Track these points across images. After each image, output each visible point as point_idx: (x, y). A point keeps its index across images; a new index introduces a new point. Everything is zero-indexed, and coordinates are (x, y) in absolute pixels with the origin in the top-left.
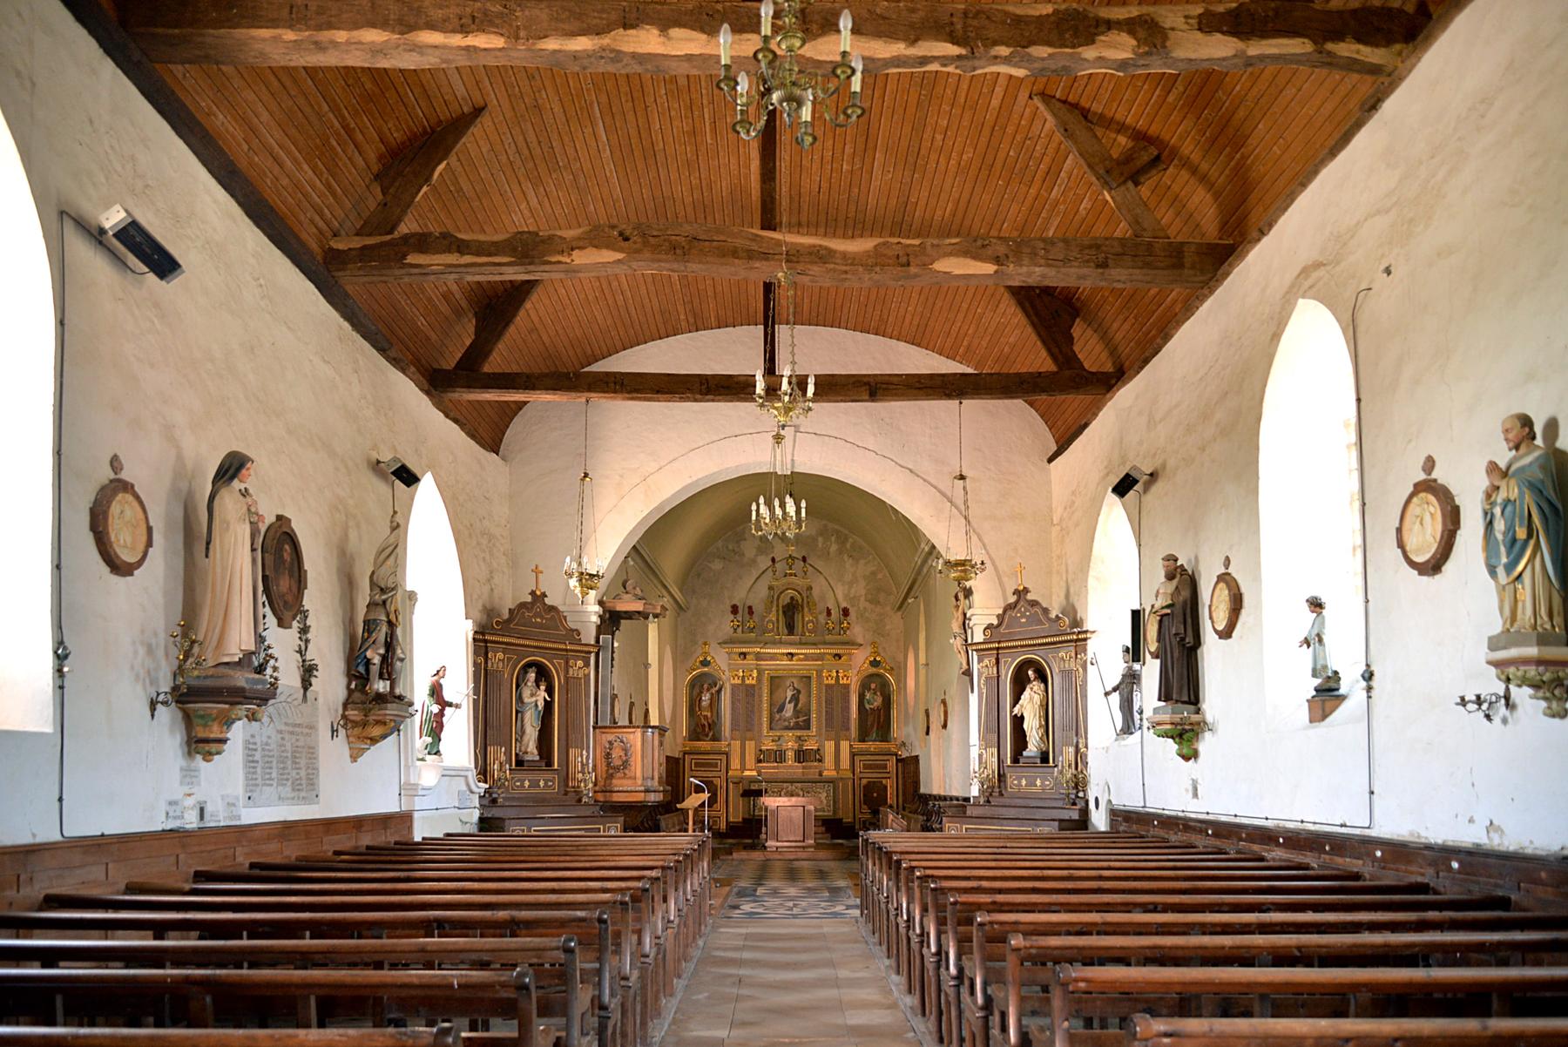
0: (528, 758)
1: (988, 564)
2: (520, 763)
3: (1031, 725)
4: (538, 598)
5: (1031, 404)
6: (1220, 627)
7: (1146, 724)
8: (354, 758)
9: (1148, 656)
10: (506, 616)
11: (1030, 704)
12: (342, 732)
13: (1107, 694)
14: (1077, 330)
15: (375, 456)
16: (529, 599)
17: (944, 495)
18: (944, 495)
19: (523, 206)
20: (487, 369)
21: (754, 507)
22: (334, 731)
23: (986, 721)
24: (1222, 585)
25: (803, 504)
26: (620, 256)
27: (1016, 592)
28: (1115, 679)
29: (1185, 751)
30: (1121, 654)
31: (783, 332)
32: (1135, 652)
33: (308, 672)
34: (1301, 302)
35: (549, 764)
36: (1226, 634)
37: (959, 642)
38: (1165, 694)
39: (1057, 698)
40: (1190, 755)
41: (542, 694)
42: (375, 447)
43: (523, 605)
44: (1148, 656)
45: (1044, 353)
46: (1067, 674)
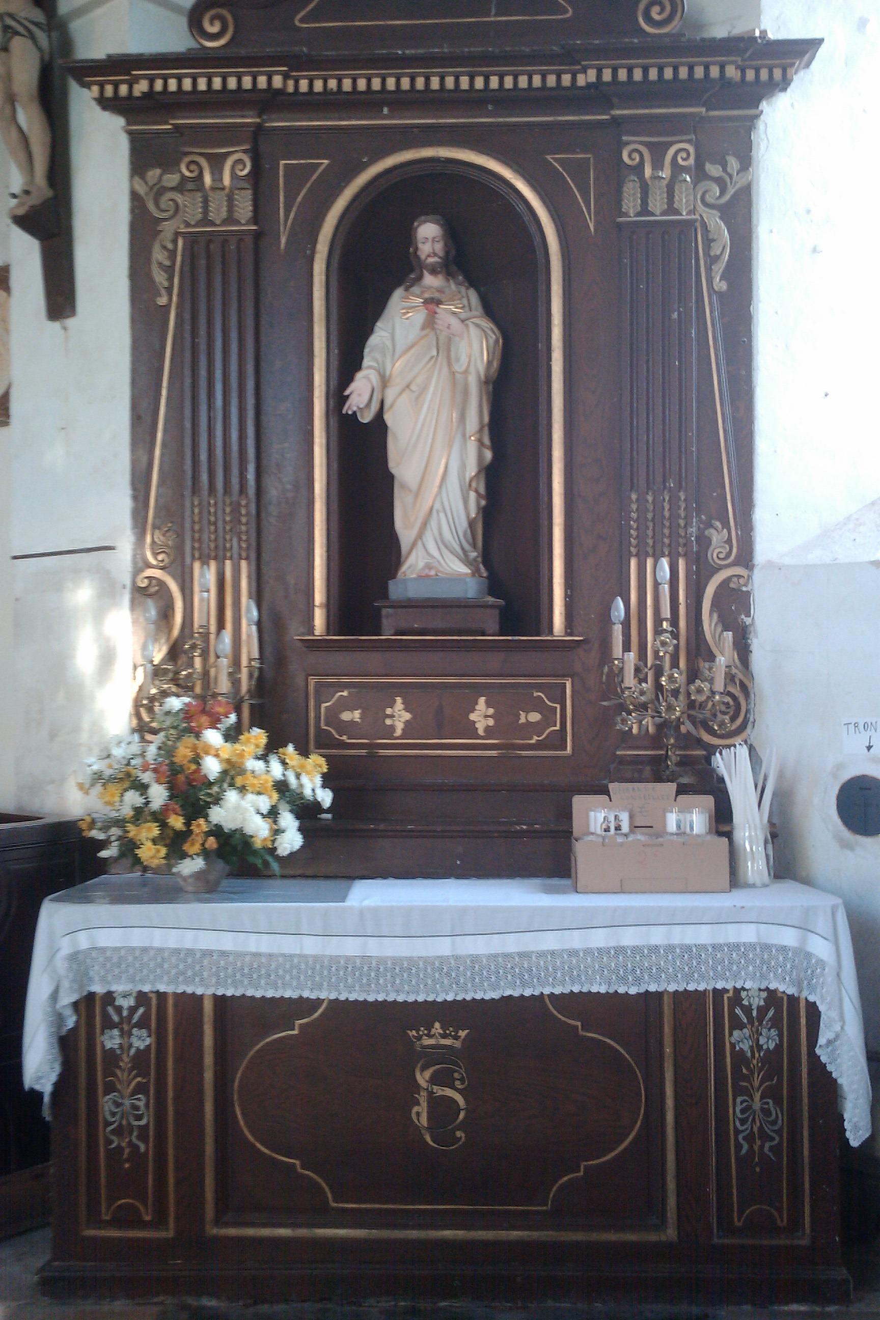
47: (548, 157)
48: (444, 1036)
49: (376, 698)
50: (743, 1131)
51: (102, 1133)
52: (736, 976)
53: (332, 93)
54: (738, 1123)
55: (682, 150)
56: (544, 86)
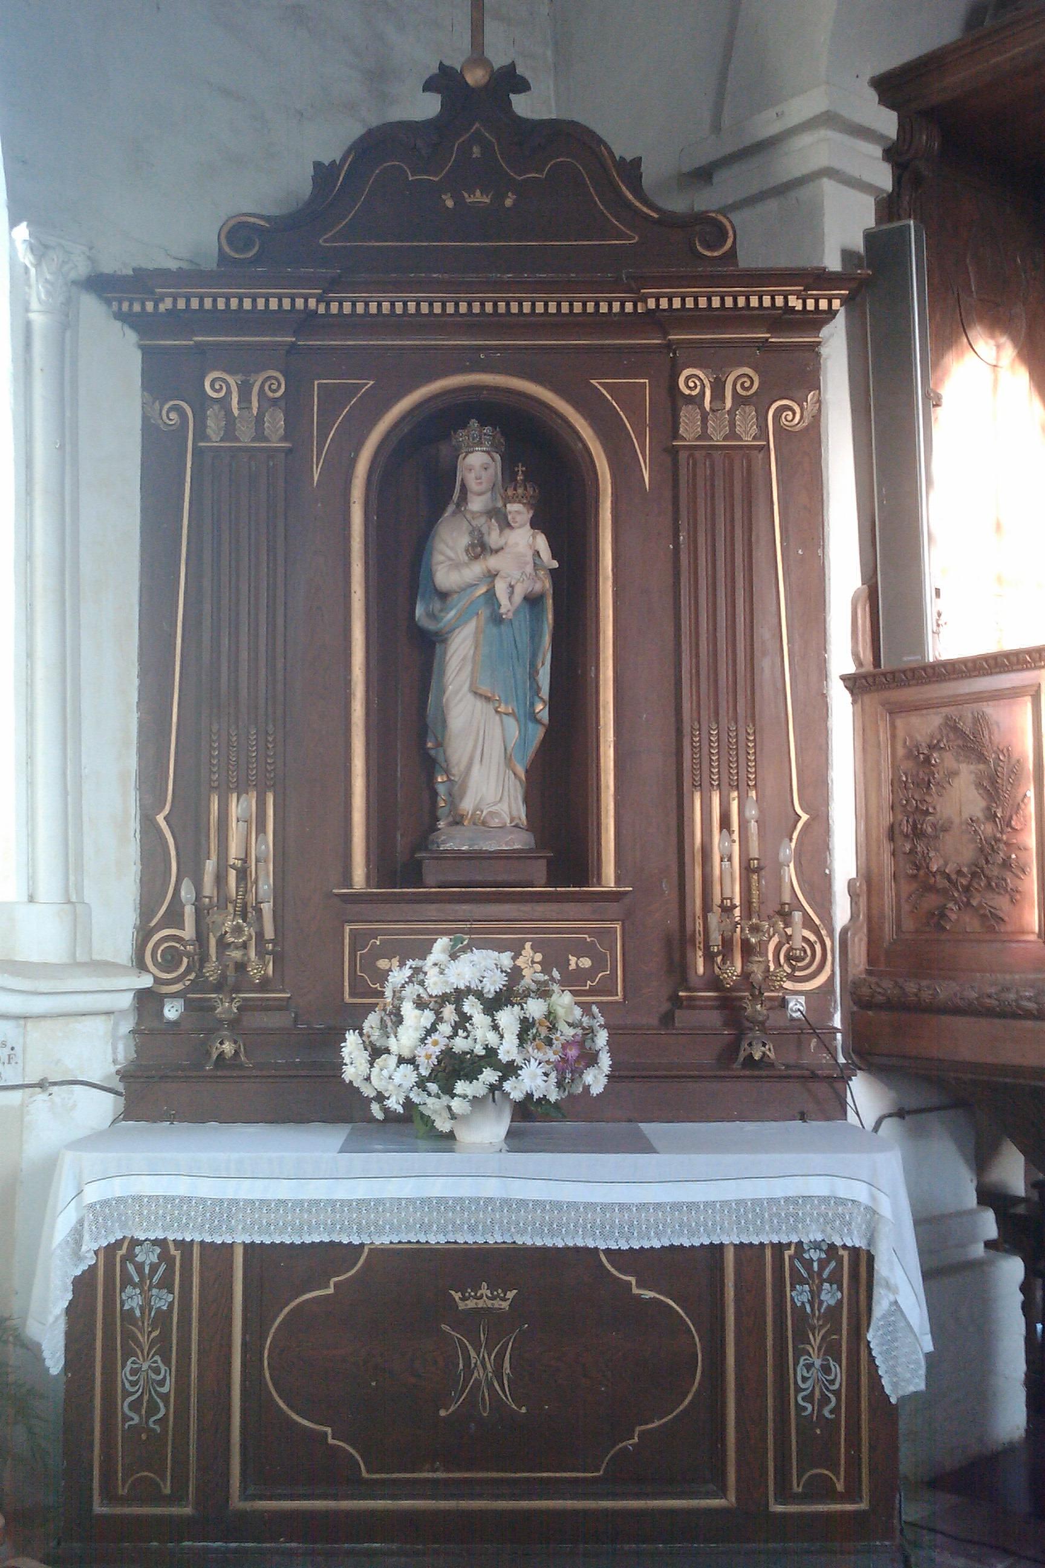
47: (372, 382)
48: (493, 1298)
50: (804, 1390)
51: (124, 1406)
52: (231, 1230)
53: (148, 314)
54: (127, 1385)
55: (742, 377)
56: (431, 313)
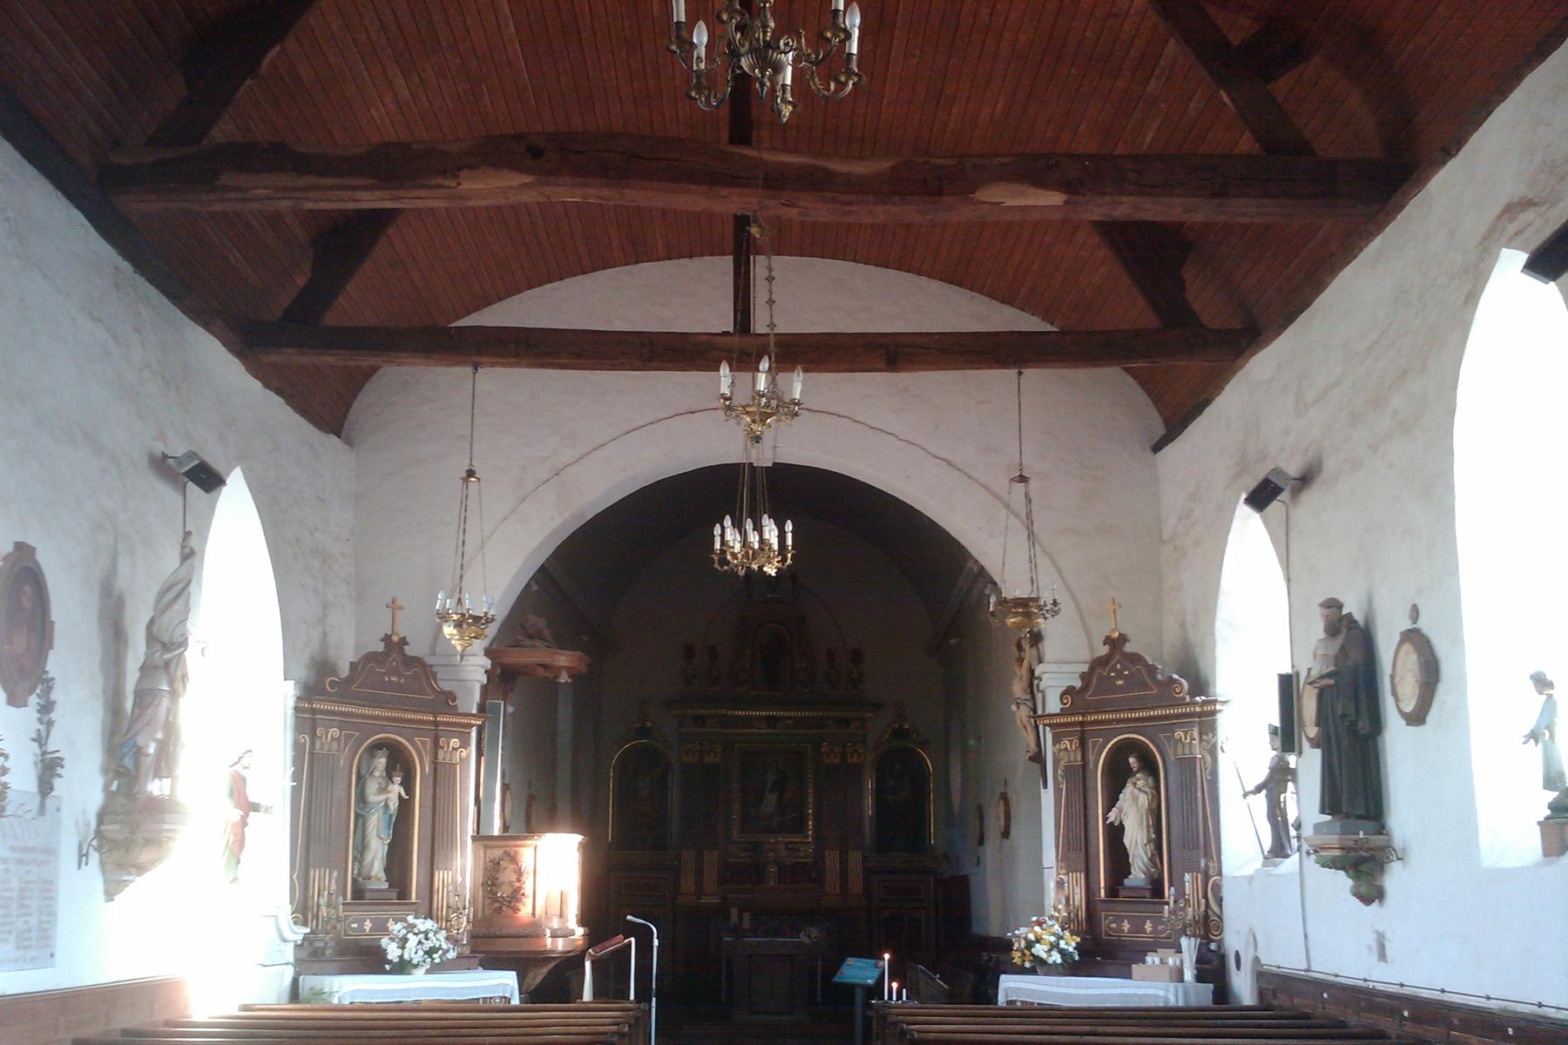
0: (373, 885)
1: (1067, 607)
2: (359, 893)
3: (1136, 839)
4: (394, 645)
5: (1127, 370)
6: (1409, 707)
7: (1305, 847)
8: (110, 895)
9: (1306, 745)
10: (345, 671)
11: (1132, 810)
12: (94, 857)
13: (1245, 795)
14: (1189, 273)
15: (159, 448)
16: (380, 647)
17: (997, 497)
18: (997, 497)
19: (388, 99)
20: (330, 319)
21: (717, 530)
22: (83, 856)
23: (1066, 836)
24: (1407, 647)
25: (789, 526)
26: (527, 179)
27: (1108, 640)
28: (1262, 774)
29: (1363, 890)
30: (1267, 737)
31: (759, 266)
32: (1286, 736)
33: (49, 769)
34: (1505, 252)
35: (403, 894)
36: (1417, 718)
37: (1023, 713)
38: (1332, 802)
39: (1173, 796)
40: (1371, 894)
41: (396, 789)
42: (161, 436)
43: (371, 657)
44: (1306, 745)
45: (1141, 302)
46: (1188, 764)
49: (1119, 920)
